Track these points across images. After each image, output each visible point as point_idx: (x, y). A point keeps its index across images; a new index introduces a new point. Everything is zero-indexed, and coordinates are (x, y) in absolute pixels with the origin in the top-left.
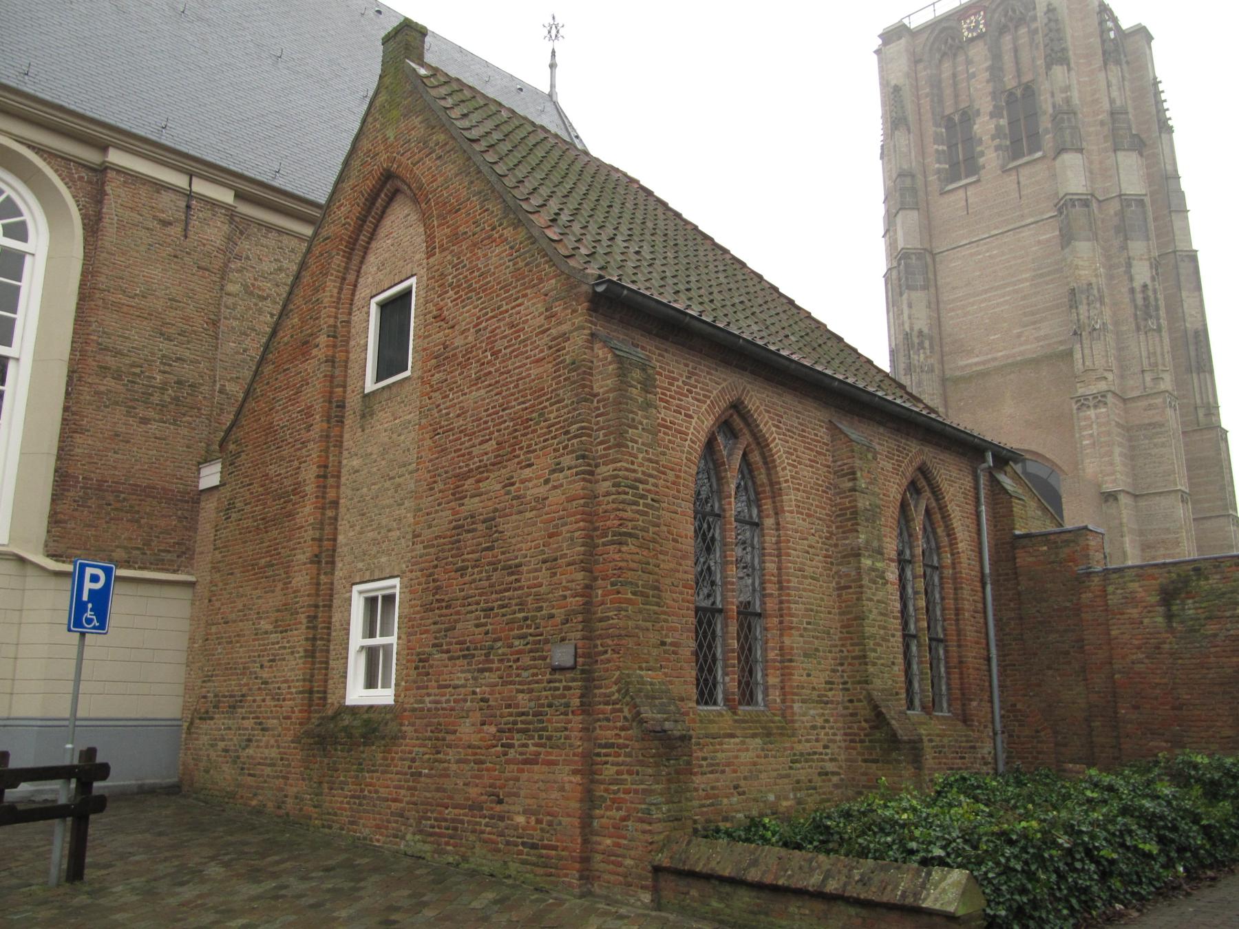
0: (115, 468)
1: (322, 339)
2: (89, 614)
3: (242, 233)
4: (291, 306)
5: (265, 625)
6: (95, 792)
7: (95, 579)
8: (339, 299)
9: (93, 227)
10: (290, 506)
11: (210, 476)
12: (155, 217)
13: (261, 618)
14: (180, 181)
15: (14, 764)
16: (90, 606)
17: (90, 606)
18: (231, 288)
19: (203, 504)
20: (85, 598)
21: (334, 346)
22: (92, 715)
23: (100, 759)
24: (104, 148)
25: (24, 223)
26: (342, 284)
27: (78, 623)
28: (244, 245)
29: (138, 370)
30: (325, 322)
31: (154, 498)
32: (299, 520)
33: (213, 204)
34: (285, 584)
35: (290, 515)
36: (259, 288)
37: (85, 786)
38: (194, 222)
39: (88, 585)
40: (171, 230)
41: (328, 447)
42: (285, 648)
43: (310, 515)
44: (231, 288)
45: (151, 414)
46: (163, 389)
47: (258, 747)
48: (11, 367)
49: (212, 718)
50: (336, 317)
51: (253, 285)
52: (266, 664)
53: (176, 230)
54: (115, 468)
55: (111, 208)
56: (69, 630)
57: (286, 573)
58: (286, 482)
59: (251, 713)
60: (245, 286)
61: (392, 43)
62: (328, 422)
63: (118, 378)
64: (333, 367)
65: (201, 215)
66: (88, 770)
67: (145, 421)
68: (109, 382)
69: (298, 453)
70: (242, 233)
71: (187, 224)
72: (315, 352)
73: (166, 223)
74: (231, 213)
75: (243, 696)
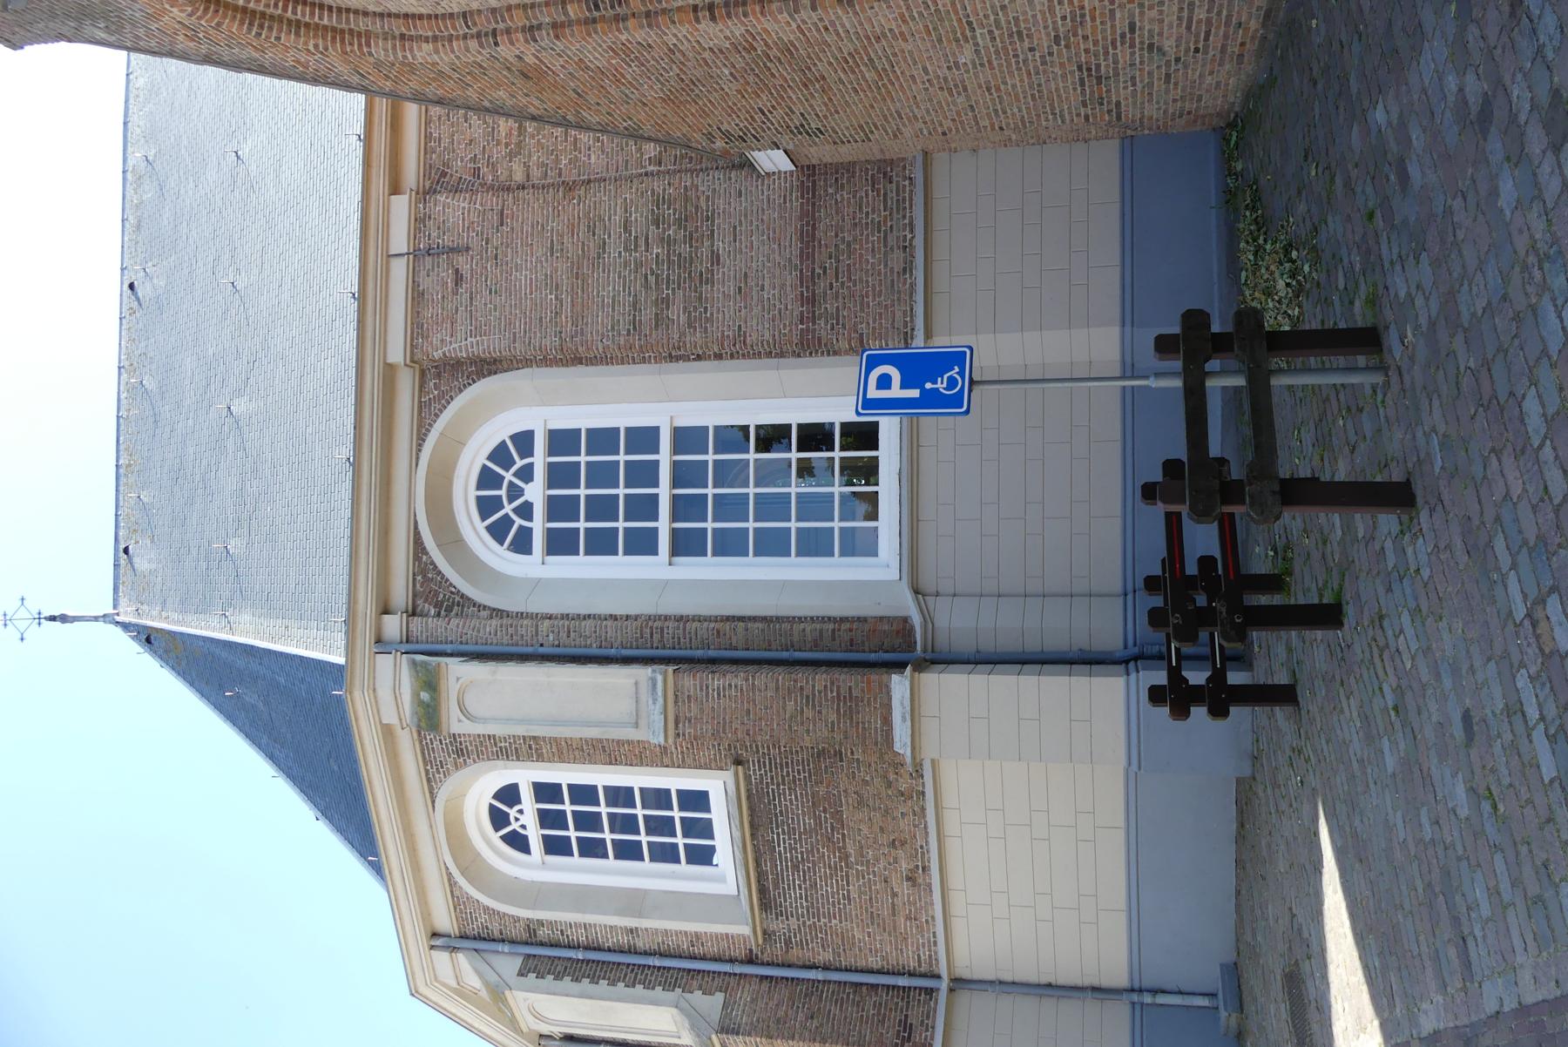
0: (783, 286)
1: (505, 51)
2: (941, 385)
3: (444, 174)
4: (486, 103)
5: (966, 56)
6: (1230, 329)
7: (884, 382)
8: (435, 39)
9: (487, 366)
10: (774, 52)
11: (773, 160)
12: (455, 293)
13: (956, 63)
14: (399, 269)
15: (1180, 452)
16: (928, 386)
17: (928, 386)
18: (519, 176)
19: (814, 162)
20: (915, 393)
21: (508, 31)
22: (1117, 261)
23: (1157, 476)
24: (389, 370)
25: (491, 458)
26: (411, 38)
27: (956, 401)
28: (459, 168)
29: (652, 279)
30: (474, 52)
31: (814, 228)
32: (789, 35)
33: (419, 222)
34: (895, 37)
35: (788, 50)
36: (509, 135)
37: (1221, 344)
38: (447, 240)
39: (896, 392)
40: (465, 269)
41: (664, 11)
42: (997, 22)
43: (777, 21)
44: (519, 176)
45: (705, 251)
46: (670, 242)
47: (1161, 34)
48: (682, 422)
49: (1118, 104)
50: (465, 37)
51: (507, 145)
52: (1026, 44)
53: (462, 262)
54: (783, 286)
55: (460, 345)
56: (967, 412)
57: (878, 39)
58: (740, 64)
59: (1106, 53)
60: (511, 156)
61: (15, 39)
62: (625, 19)
63: (666, 302)
64: (539, 27)
65: (434, 234)
66: (1191, 344)
67: (716, 258)
68: (676, 313)
69: (691, 55)
70: (444, 174)
71: (452, 250)
72: (530, 59)
73: (458, 278)
74: (424, 195)
75: (1080, 68)
